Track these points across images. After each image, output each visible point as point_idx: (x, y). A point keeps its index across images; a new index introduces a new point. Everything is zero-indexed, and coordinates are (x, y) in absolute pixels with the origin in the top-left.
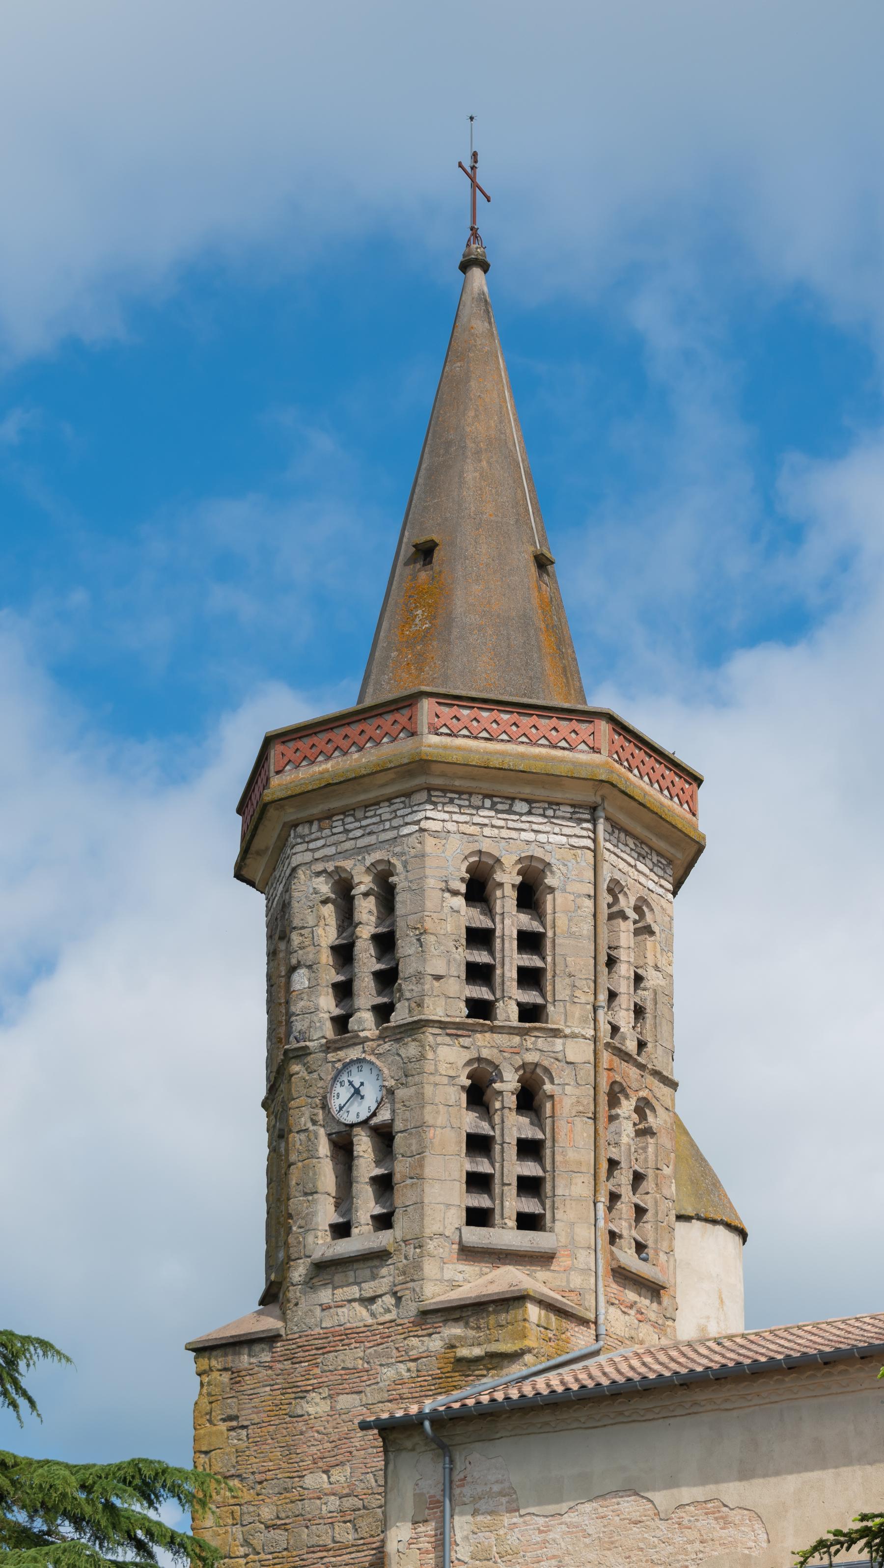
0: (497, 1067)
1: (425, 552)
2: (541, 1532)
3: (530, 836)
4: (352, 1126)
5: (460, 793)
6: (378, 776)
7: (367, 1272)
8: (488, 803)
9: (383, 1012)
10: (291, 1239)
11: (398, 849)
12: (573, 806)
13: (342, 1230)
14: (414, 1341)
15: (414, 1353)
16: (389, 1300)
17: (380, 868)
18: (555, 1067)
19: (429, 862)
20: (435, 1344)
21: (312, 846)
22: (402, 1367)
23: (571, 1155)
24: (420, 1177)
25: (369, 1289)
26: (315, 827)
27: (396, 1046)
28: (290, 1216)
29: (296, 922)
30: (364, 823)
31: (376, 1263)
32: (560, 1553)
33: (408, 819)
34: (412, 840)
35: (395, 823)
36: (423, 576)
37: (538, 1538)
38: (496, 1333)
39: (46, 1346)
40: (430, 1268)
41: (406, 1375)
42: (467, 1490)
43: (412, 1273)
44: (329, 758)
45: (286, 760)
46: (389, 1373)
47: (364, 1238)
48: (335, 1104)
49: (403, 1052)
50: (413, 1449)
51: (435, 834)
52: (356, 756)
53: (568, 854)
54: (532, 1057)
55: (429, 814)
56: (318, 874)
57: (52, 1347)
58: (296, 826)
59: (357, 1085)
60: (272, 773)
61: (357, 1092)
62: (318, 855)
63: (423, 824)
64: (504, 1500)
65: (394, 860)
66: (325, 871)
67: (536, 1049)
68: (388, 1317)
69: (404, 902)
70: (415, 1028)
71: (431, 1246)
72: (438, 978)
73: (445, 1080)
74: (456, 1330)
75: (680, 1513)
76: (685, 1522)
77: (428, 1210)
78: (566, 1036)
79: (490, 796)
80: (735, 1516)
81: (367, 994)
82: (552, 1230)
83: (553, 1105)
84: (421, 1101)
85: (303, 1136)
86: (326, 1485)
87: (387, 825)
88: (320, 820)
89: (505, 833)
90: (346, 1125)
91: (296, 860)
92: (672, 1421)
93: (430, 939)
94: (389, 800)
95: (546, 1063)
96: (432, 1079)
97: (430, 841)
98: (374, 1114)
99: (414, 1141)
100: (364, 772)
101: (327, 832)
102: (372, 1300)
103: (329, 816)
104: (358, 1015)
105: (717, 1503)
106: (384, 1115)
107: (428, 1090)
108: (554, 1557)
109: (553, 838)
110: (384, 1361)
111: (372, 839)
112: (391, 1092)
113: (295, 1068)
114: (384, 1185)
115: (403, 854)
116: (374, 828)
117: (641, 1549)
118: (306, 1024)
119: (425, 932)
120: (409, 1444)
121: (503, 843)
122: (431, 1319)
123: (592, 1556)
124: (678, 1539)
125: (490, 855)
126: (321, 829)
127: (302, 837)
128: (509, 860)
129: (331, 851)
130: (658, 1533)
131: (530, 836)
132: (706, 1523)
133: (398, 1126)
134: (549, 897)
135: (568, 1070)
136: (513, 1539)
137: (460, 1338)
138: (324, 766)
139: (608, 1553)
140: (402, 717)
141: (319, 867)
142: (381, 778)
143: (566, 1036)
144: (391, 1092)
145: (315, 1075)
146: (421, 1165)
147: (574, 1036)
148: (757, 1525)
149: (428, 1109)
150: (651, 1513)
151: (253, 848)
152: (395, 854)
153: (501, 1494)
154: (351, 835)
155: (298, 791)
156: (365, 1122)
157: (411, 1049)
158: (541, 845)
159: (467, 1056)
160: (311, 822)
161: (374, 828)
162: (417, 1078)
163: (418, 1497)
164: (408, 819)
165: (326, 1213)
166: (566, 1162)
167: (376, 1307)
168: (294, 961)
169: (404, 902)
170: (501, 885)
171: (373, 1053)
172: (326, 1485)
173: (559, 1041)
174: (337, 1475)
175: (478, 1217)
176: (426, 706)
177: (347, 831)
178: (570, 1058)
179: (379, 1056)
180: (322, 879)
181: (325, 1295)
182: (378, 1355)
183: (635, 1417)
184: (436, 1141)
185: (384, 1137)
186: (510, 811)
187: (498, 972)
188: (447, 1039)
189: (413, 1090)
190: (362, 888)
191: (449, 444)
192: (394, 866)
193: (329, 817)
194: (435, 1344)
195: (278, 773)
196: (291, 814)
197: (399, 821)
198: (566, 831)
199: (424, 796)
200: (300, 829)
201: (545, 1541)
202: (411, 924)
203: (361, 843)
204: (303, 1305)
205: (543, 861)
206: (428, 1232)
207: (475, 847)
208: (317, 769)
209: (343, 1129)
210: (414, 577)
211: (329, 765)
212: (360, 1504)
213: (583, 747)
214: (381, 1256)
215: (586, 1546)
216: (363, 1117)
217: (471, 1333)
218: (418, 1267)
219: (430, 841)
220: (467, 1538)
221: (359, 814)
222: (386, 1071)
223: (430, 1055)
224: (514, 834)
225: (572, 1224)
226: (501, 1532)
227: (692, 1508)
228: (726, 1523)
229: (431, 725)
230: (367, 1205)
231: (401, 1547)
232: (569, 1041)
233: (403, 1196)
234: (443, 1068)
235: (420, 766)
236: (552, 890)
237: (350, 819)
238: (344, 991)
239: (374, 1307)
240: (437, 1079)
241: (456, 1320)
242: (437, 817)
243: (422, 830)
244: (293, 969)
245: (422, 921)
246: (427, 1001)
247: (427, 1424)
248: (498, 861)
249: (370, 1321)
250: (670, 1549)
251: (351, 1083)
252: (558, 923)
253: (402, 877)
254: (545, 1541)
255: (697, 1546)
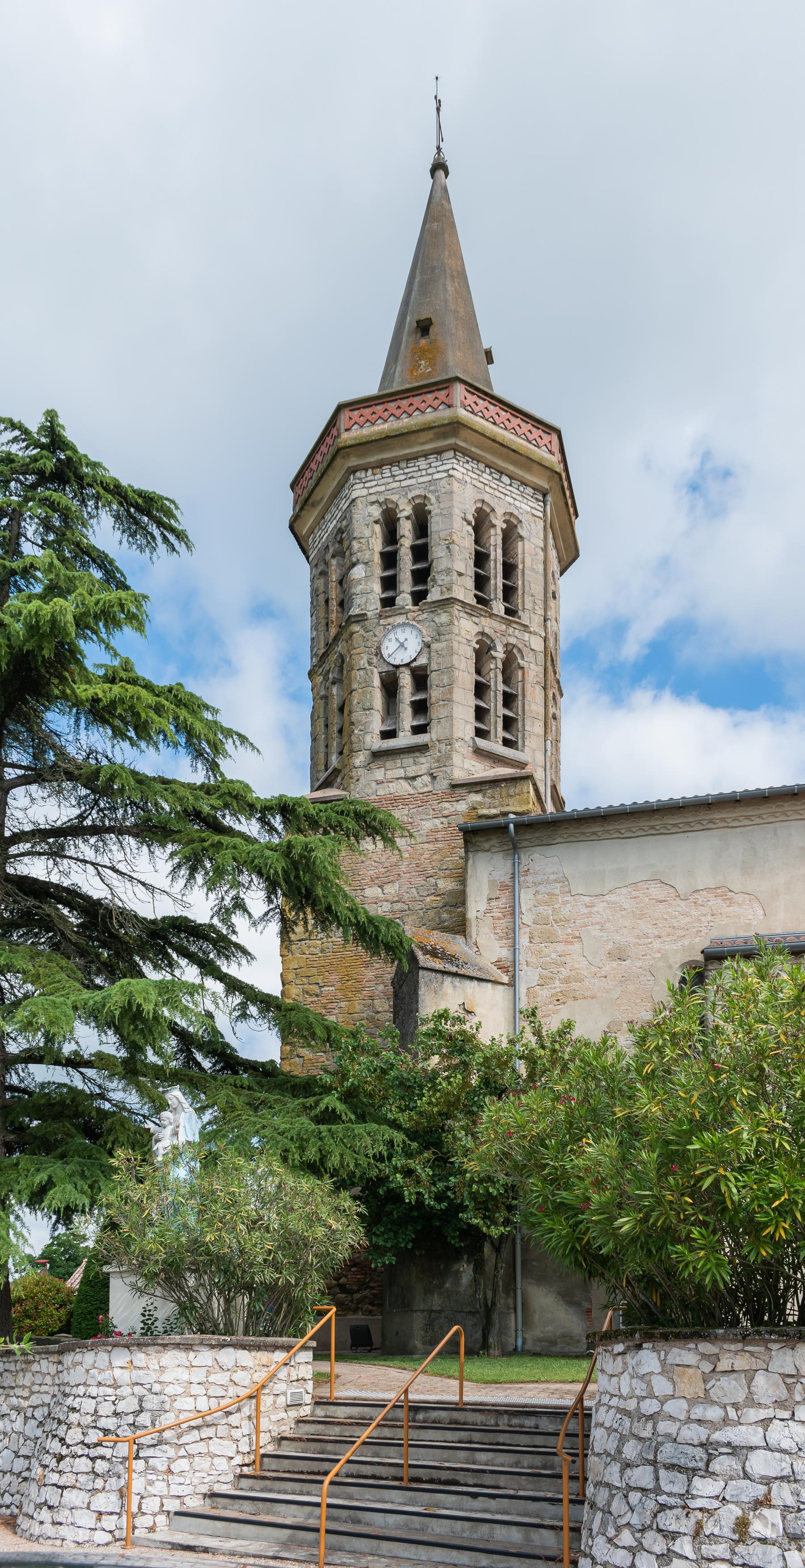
0: (493, 641)
1: (424, 327)
2: (587, 907)
3: (511, 501)
4: (397, 667)
5: (473, 459)
6: (422, 434)
7: (411, 760)
8: (488, 470)
9: (418, 597)
10: (354, 738)
11: (432, 488)
12: (534, 489)
13: (388, 735)
14: (447, 805)
15: (446, 812)
16: (427, 779)
17: (417, 501)
18: (525, 651)
19: (455, 497)
20: (462, 807)
21: (367, 485)
22: (437, 821)
23: (533, 707)
24: (450, 700)
25: (412, 771)
26: (370, 472)
27: (432, 615)
28: (353, 724)
29: (356, 534)
30: (406, 471)
31: (417, 754)
32: (602, 921)
33: (440, 469)
34: (443, 482)
35: (430, 471)
36: (423, 342)
37: (585, 911)
38: (506, 801)
39: (243, 739)
40: (456, 759)
41: (441, 826)
42: (529, 878)
43: (445, 760)
44: (386, 421)
45: (352, 422)
46: (427, 825)
47: (405, 739)
48: (385, 653)
49: (437, 619)
50: (488, 851)
51: (458, 480)
52: (406, 420)
53: (532, 519)
54: (513, 640)
55: (455, 466)
56: (373, 503)
57: (247, 739)
58: (354, 472)
59: (402, 640)
60: (342, 430)
61: (402, 645)
62: (371, 491)
63: (451, 472)
64: (558, 885)
65: (429, 495)
66: (377, 502)
67: (515, 636)
68: (426, 789)
69: (437, 523)
70: (446, 603)
71: (457, 745)
72: (460, 574)
73: (465, 641)
74: (477, 798)
75: (696, 895)
76: (700, 902)
77: (455, 722)
78: (530, 632)
79: (490, 467)
80: (739, 898)
81: (406, 585)
82: (523, 751)
83: (523, 675)
84: (451, 652)
85: (362, 673)
86: (381, 895)
87: (424, 473)
88: (373, 468)
89: (497, 494)
90: (394, 666)
91: (354, 495)
92: (689, 834)
93: (454, 548)
94: (426, 455)
95: (520, 646)
96: (457, 638)
97: (456, 485)
98: (415, 660)
99: (445, 677)
100: (414, 428)
101: (379, 476)
102: (414, 778)
103: (380, 465)
104: (402, 595)
105: (724, 889)
106: (422, 661)
107: (455, 645)
108: (598, 923)
109: (523, 506)
110: (424, 817)
111: (413, 481)
112: (428, 646)
113: (356, 628)
114: (420, 708)
115: (436, 491)
116: (414, 474)
117: (666, 919)
118: (364, 600)
119: (453, 542)
120: (487, 846)
121: (496, 500)
122: (459, 791)
123: (626, 923)
124: (694, 913)
125: (489, 505)
126: (374, 474)
127: (360, 479)
128: (500, 511)
129: (382, 488)
130: (679, 909)
131: (511, 501)
132: (716, 903)
133: (434, 666)
134: (520, 544)
135: (531, 654)
136: (566, 911)
137: (480, 803)
138: (382, 427)
139: (640, 921)
140: (442, 394)
141: (373, 498)
142: (424, 436)
143: (530, 632)
144: (428, 646)
145: (371, 633)
146: (451, 692)
147: (535, 633)
148: (756, 905)
149: (455, 657)
150: (673, 895)
151: (311, 500)
152: (430, 491)
153: (556, 881)
154: (397, 478)
155: (364, 440)
156: (407, 665)
157: (443, 618)
158: (517, 508)
159: (477, 629)
160: (366, 470)
161: (414, 474)
162: (447, 637)
163: (492, 883)
164: (440, 469)
165: (377, 724)
166: (530, 711)
167: (418, 783)
168: (354, 560)
169: (437, 523)
170: (494, 526)
171: (414, 619)
172: (381, 895)
173: (527, 635)
174: (388, 889)
175: (481, 733)
176: (459, 390)
177: (394, 476)
178: (533, 647)
179: (419, 622)
180: (375, 507)
181: (379, 774)
182: (419, 813)
183: (663, 831)
184: (460, 678)
185: (421, 679)
186: (499, 480)
187: (492, 582)
188: (465, 615)
189: (444, 644)
190: (406, 514)
191: (433, 269)
192: (429, 499)
193: (380, 467)
194: (462, 807)
195: (347, 430)
196: (353, 462)
197: (434, 470)
198: (530, 503)
199: (451, 454)
200: (358, 474)
201: (591, 913)
202: (443, 537)
203: (404, 484)
204: (362, 781)
205: (517, 518)
206: (455, 736)
207: (480, 497)
208: (376, 428)
209: (391, 668)
210: (417, 342)
211: (386, 426)
212: (406, 907)
213: (544, 448)
214: (422, 749)
215: (623, 916)
216: (405, 662)
217: (488, 800)
218: (449, 757)
219: (456, 485)
220: (530, 909)
221: (403, 465)
222: (424, 631)
223: (456, 623)
224: (502, 496)
225: (534, 751)
226: (557, 906)
227: (705, 893)
228: (731, 902)
229: (462, 402)
230: (407, 719)
231: (479, 915)
232: (532, 637)
233: (436, 712)
234: (463, 633)
235: (455, 426)
236: (521, 538)
237: (396, 468)
238: (390, 583)
239: (415, 783)
240: (460, 639)
241: (477, 792)
242: (461, 469)
243: (450, 476)
244: (354, 565)
245: (450, 535)
246: (455, 587)
247: (512, 826)
248: (493, 510)
249: (412, 792)
250: (688, 919)
251: (397, 639)
252: (526, 560)
253: (436, 506)
254: (591, 913)
255: (709, 918)
